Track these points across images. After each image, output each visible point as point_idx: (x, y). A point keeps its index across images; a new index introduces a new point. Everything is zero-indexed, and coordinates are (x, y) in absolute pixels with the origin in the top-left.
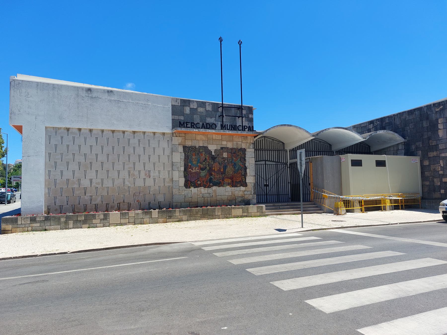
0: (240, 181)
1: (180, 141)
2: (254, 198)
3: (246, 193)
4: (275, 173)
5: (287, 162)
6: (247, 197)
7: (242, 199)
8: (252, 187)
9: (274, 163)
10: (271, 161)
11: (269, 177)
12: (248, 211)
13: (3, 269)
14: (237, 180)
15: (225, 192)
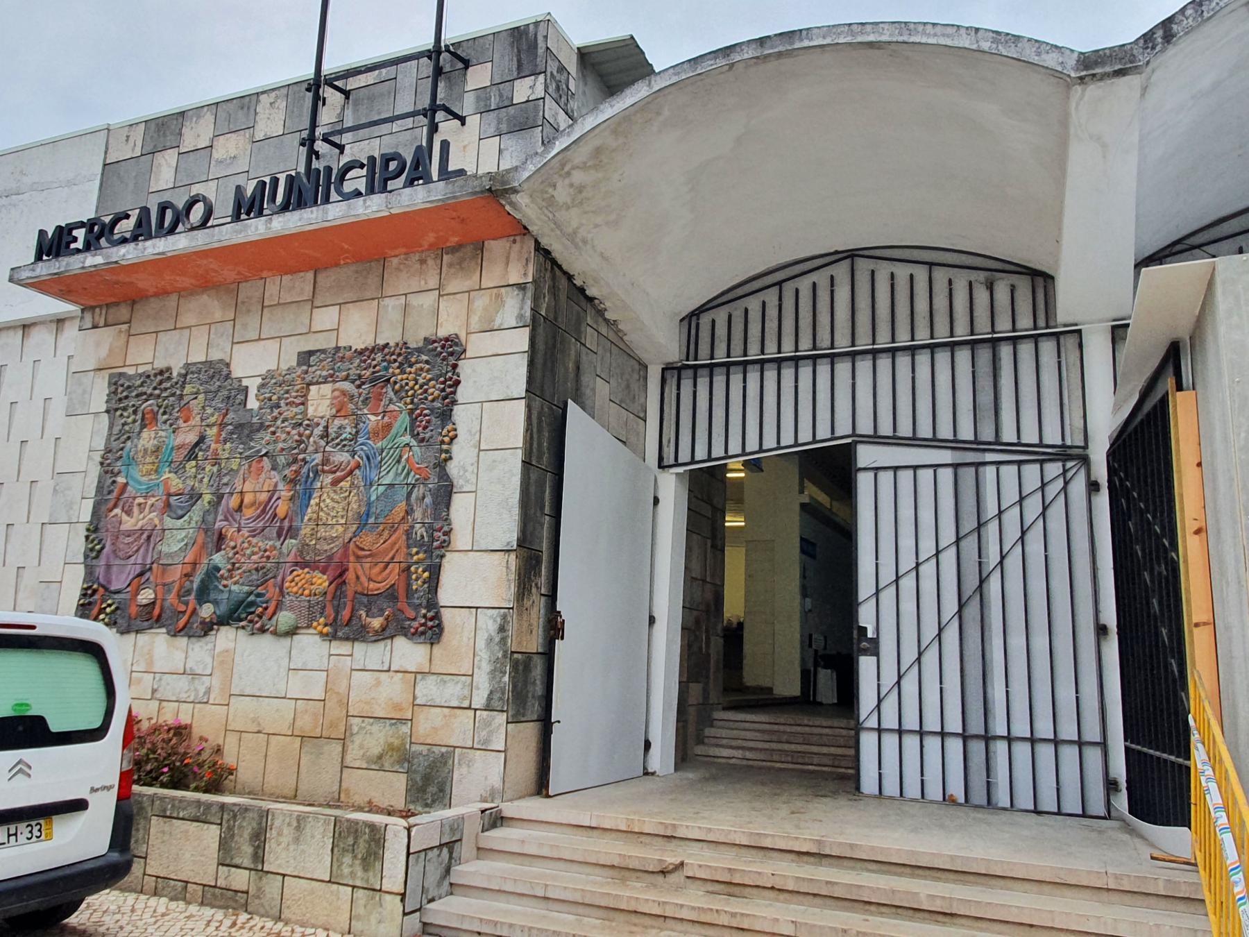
0: (391, 595)
1: (103, 352)
2: (487, 741)
3: (427, 690)
4: (948, 536)
5: (663, 381)
6: (435, 729)
7: (397, 742)
8: (481, 644)
9: (946, 456)
10: (914, 441)
11: (887, 575)
12: (259, 856)
13: (1210, 772)
14: (372, 585)
15: (283, 672)
